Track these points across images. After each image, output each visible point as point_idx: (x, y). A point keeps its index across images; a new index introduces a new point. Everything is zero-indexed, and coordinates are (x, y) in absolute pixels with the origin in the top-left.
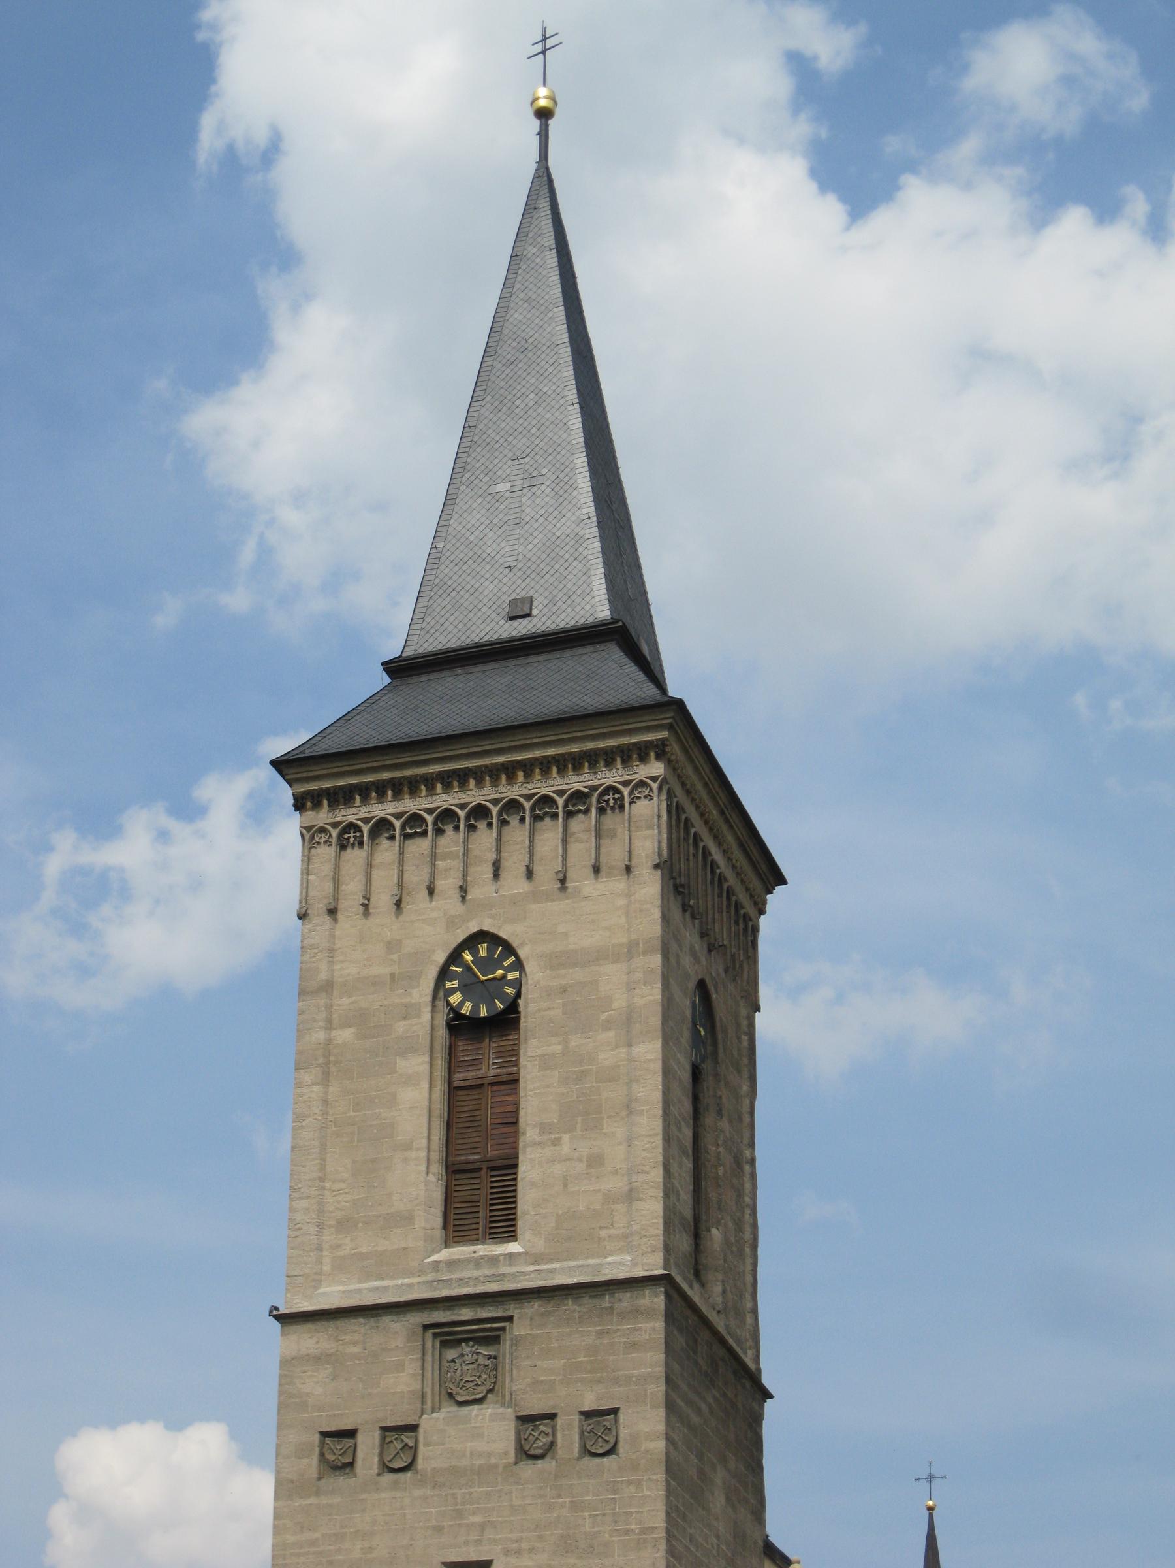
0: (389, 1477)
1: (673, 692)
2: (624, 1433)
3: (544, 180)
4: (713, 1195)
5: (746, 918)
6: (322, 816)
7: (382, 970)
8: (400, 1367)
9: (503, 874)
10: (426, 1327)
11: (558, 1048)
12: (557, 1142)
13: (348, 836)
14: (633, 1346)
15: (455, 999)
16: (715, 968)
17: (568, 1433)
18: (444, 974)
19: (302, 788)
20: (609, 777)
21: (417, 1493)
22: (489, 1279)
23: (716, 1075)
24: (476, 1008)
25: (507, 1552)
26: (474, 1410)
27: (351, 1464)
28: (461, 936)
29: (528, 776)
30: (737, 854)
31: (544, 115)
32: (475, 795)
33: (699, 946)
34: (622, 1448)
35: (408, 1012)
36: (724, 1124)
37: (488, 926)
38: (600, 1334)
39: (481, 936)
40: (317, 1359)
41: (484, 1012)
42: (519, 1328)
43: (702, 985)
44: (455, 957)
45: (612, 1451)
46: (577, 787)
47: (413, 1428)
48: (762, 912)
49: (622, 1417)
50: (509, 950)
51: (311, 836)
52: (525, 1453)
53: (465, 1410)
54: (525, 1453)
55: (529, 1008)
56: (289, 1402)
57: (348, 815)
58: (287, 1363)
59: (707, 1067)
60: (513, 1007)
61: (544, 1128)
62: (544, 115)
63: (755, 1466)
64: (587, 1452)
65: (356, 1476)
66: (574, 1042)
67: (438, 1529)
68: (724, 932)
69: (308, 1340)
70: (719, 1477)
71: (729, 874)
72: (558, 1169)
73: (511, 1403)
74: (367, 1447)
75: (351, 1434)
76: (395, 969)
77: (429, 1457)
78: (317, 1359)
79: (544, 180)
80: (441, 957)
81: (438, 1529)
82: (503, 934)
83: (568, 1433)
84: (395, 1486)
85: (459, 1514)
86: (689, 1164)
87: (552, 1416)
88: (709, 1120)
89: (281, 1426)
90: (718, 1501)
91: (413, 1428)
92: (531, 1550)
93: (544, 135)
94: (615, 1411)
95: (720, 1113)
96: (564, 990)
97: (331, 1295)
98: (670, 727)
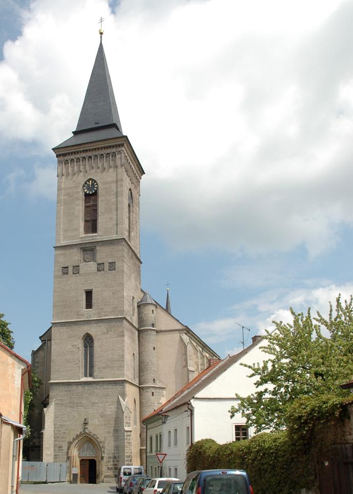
0: (74, 275)
1: (124, 134)
2: (116, 266)
3: (101, 45)
4: (132, 227)
5: (138, 179)
6: (61, 158)
7: (72, 186)
8: (76, 255)
9: (155, 381)
10: (81, 248)
11: (104, 199)
12: (104, 215)
13: (66, 162)
14: (118, 251)
15: (86, 190)
16: (132, 187)
17: (107, 267)
18: (84, 186)
19: (57, 153)
20: (114, 150)
21: (80, 277)
22: (92, 239)
23: (133, 206)
24: (89, 192)
25: (95, 288)
26: (89, 263)
27: (68, 273)
28: (87, 179)
29: (98, 150)
30: (136, 167)
31: (101, 34)
32: (89, 154)
33: (130, 182)
34: (116, 269)
35: (77, 193)
36: (134, 214)
37: (91, 178)
38: (112, 249)
39: (90, 179)
40: (61, 254)
41: (91, 193)
42: (98, 248)
43: (130, 189)
44: (86, 183)
45: (114, 269)
46: (108, 152)
47: (79, 266)
48: (141, 179)
49: (116, 263)
50: (95, 182)
51: (59, 162)
52: (99, 270)
53: (87, 263)
54: (99, 270)
55: (100, 192)
56: (56, 262)
57: (66, 158)
58: (56, 255)
59: (131, 204)
60: (96, 192)
61: (102, 213)
62: (101, 34)
63: (139, 275)
64: (110, 270)
65: (85, 290)
66: (107, 197)
67: (83, 284)
68: (134, 180)
69: (60, 252)
70: (133, 275)
71: (135, 171)
72: (104, 220)
73: (96, 262)
74: (70, 270)
75: (67, 267)
76: (75, 185)
77: (81, 271)
78: (61, 254)
79: (101, 45)
80: (83, 183)
81: (83, 284)
82: (94, 179)
83: (107, 267)
84: (75, 276)
85: (87, 281)
86: (128, 220)
87: (103, 263)
88: (131, 214)
89: (55, 266)
90: (133, 280)
91: (79, 266)
92: (100, 287)
93: (101, 37)
94: (115, 262)
95: (133, 213)
96: (105, 188)
97: (63, 243)
98: (125, 141)
